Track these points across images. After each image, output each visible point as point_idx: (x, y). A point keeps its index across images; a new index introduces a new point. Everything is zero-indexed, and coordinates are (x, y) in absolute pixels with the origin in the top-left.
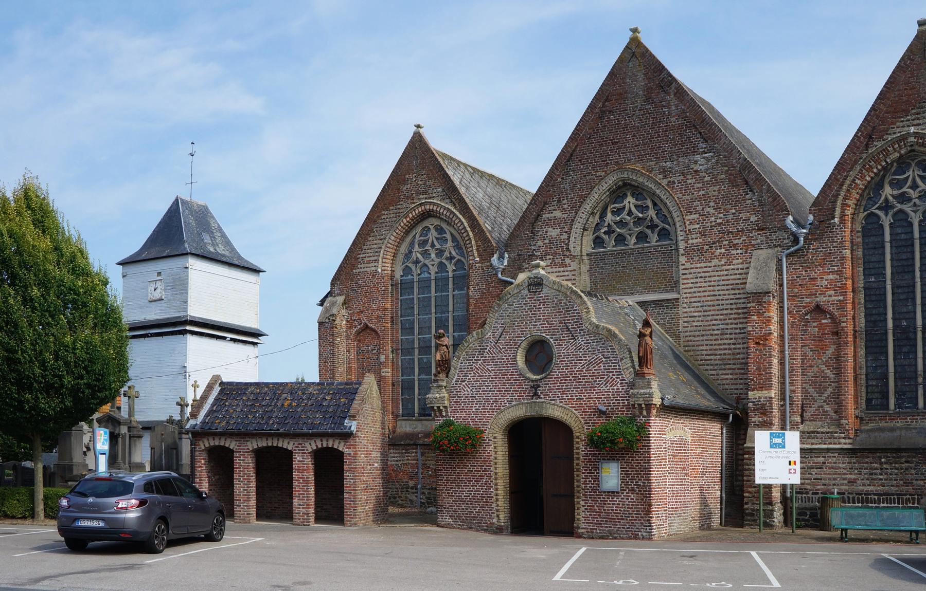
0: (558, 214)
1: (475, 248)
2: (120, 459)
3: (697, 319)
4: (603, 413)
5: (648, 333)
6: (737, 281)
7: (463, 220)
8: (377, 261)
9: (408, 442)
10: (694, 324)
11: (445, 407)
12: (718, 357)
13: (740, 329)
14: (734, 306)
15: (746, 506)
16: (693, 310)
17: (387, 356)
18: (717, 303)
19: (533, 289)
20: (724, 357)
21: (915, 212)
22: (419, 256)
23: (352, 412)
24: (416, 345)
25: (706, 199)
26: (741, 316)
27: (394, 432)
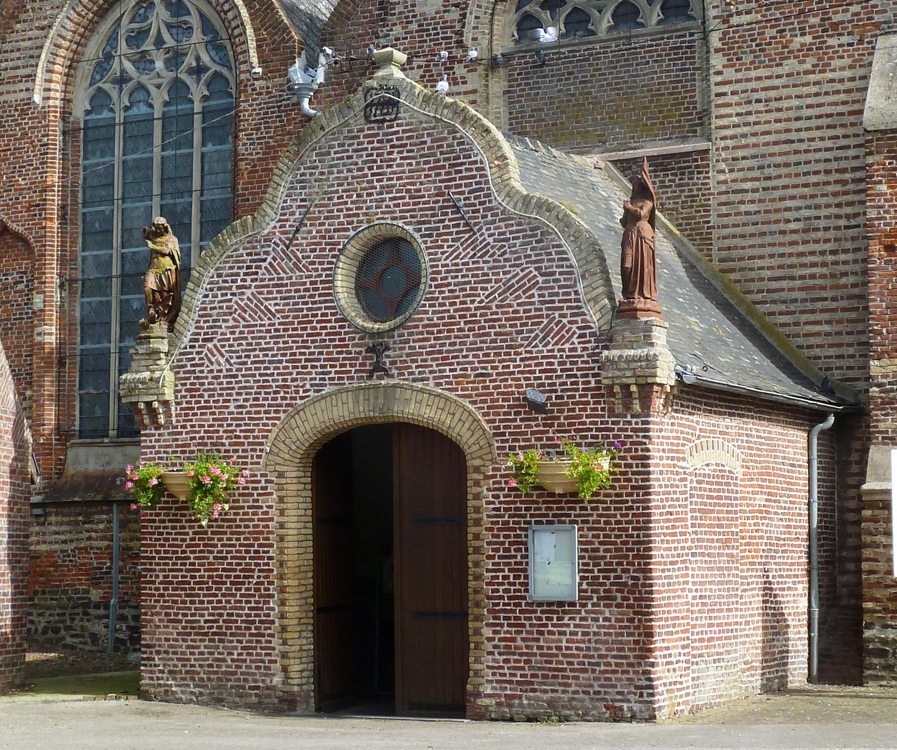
1: (252, 45)
3: (750, 196)
5: (645, 212)
6: (841, 109)
8: (31, 77)
9: (91, 496)
10: (743, 208)
11: (166, 403)
12: (798, 283)
13: (848, 217)
14: (834, 165)
15: (867, 634)
16: (740, 175)
18: (793, 158)
19: (377, 114)
20: (811, 282)
21: (158, 87)
22: (128, 65)
24: (115, 270)
26: (851, 187)
27: (60, 474)
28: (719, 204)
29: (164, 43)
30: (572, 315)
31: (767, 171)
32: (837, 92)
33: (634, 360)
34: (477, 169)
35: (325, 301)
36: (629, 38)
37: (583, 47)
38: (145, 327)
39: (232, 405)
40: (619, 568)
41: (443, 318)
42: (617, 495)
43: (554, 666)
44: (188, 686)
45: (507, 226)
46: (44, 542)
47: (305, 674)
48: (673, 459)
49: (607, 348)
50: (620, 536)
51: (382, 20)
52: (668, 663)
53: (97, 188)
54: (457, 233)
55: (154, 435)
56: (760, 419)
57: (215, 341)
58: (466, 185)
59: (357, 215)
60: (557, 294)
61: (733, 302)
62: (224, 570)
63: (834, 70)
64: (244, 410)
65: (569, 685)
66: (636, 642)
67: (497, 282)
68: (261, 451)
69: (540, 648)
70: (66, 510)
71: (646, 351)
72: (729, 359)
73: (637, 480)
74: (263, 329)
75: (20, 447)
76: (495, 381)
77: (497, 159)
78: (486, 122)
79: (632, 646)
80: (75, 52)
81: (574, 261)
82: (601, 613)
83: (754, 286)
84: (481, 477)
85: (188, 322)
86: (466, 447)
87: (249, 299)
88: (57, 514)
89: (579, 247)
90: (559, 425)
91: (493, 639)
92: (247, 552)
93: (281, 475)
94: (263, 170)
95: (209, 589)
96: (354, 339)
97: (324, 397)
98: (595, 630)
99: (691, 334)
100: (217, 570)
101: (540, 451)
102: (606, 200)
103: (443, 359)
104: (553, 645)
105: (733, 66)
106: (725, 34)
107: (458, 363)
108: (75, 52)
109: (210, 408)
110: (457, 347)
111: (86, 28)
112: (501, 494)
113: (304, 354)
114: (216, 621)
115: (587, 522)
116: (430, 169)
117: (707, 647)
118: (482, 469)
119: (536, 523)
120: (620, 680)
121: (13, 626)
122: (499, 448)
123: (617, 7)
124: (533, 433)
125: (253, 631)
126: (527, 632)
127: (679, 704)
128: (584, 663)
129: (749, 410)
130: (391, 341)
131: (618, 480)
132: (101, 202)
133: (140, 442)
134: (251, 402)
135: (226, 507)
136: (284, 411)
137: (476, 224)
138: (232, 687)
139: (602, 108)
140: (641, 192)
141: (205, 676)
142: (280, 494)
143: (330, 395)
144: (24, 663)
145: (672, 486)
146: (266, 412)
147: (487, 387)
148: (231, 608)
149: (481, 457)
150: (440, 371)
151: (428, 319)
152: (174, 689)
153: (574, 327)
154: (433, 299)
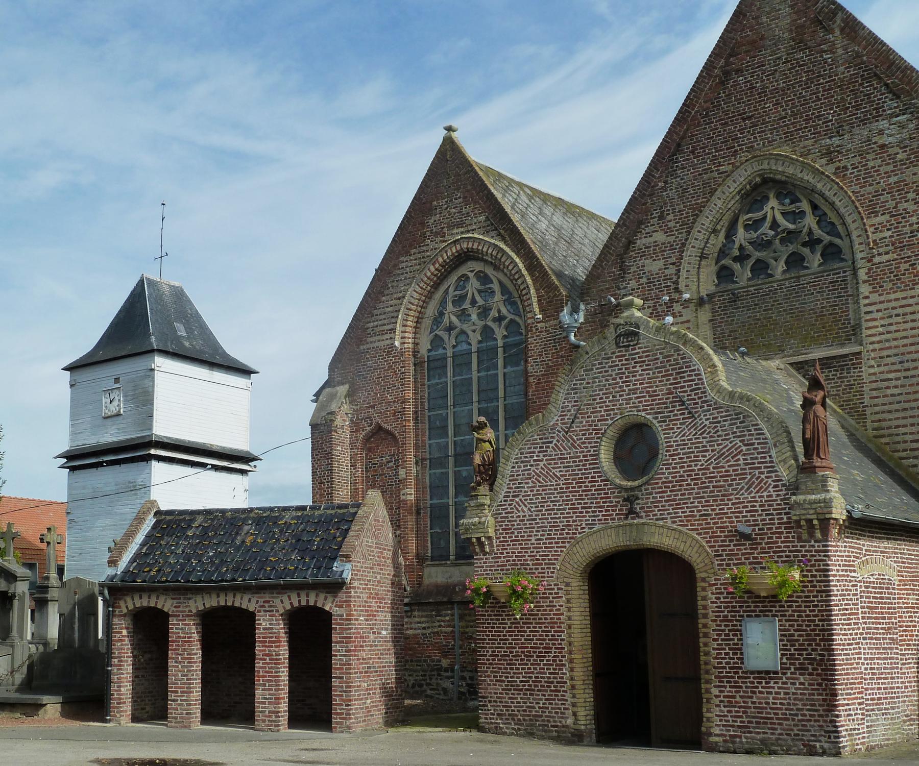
0: (660, 237)
1: (535, 300)
2: (14, 633)
3: (894, 383)
4: (747, 537)
5: (818, 399)
7: (517, 260)
8: (393, 330)
9: (440, 599)
10: (889, 392)
11: (489, 538)
16: (886, 368)
17: (410, 470)
19: (624, 341)
21: (474, 331)
22: (454, 319)
23: (344, 550)
24: (451, 452)
25: (901, 189)
27: (420, 584)
28: (871, 390)
29: (476, 302)
30: (768, 472)
31: (906, 365)
33: (811, 503)
34: (696, 375)
35: (594, 468)
36: (798, 277)
37: (764, 286)
38: (474, 489)
39: (533, 539)
40: (810, 648)
41: (676, 477)
42: (806, 597)
43: (764, 715)
44: (510, 724)
45: (718, 413)
46: (411, 629)
47: (588, 717)
48: (846, 571)
49: (794, 494)
50: (810, 626)
51: (622, 277)
52: (849, 715)
53: (438, 398)
54: (683, 419)
56: (910, 541)
57: (521, 497)
58: (689, 386)
59: (613, 410)
60: (757, 458)
61: (884, 459)
62: (531, 648)
65: (776, 729)
66: (824, 700)
67: (713, 451)
69: (753, 703)
70: (425, 608)
71: (823, 496)
72: (885, 499)
73: (820, 586)
75: (397, 568)
77: (709, 367)
78: (700, 342)
79: (821, 703)
80: (420, 312)
81: (768, 435)
82: (797, 679)
83: (900, 447)
84: (707, 584)
85: (503, 484)
86: (695, 564)
88: (418, 611)
89: (771, 425)
90: (762, 548)
91: (719, 696)
92: (547, 636)
93: (567, 585)
94: (545, 382)
95: (522, 660)
97: (595, 532)
98: (794, 691)
99: (854, 483)
100: (527, 647)
101: (749, 567)
102: (787, 390)
103: (677, 504)
105: (878, 291)
106: (870, 269)
108: (420, 312)
109: (519, 541)
111: (426, 297)
112: (721, 596)
113: (580, 504)
114: (528, 681)
115: (785, 615)
116: (662, 376)
117: (877, 704)
119: (748, 616)
120: (813, 726)
121: (396, 683)
122: (719, 565)
123: (789, 257)
124: (743, 554)
125: (553, 688)
126: (744, 692)
127: (857, 744)
129: (902, 536)
131: (807, 586)
132: (440, 407)
133: (474, 563)
135: (532, 606)
137: (696, 412)
138: (540, 725)
139: (781, 327)
140: (815, 384)
142: (568, 597)
143: (599, 530)
144: (404, 707)
145: (847, 590)
146: (556, 543)
147: (709, 524)
149: (706, 571)
150: (675, 513)
151: (666, 478)
153: (770, 480)
154: (668, 464)
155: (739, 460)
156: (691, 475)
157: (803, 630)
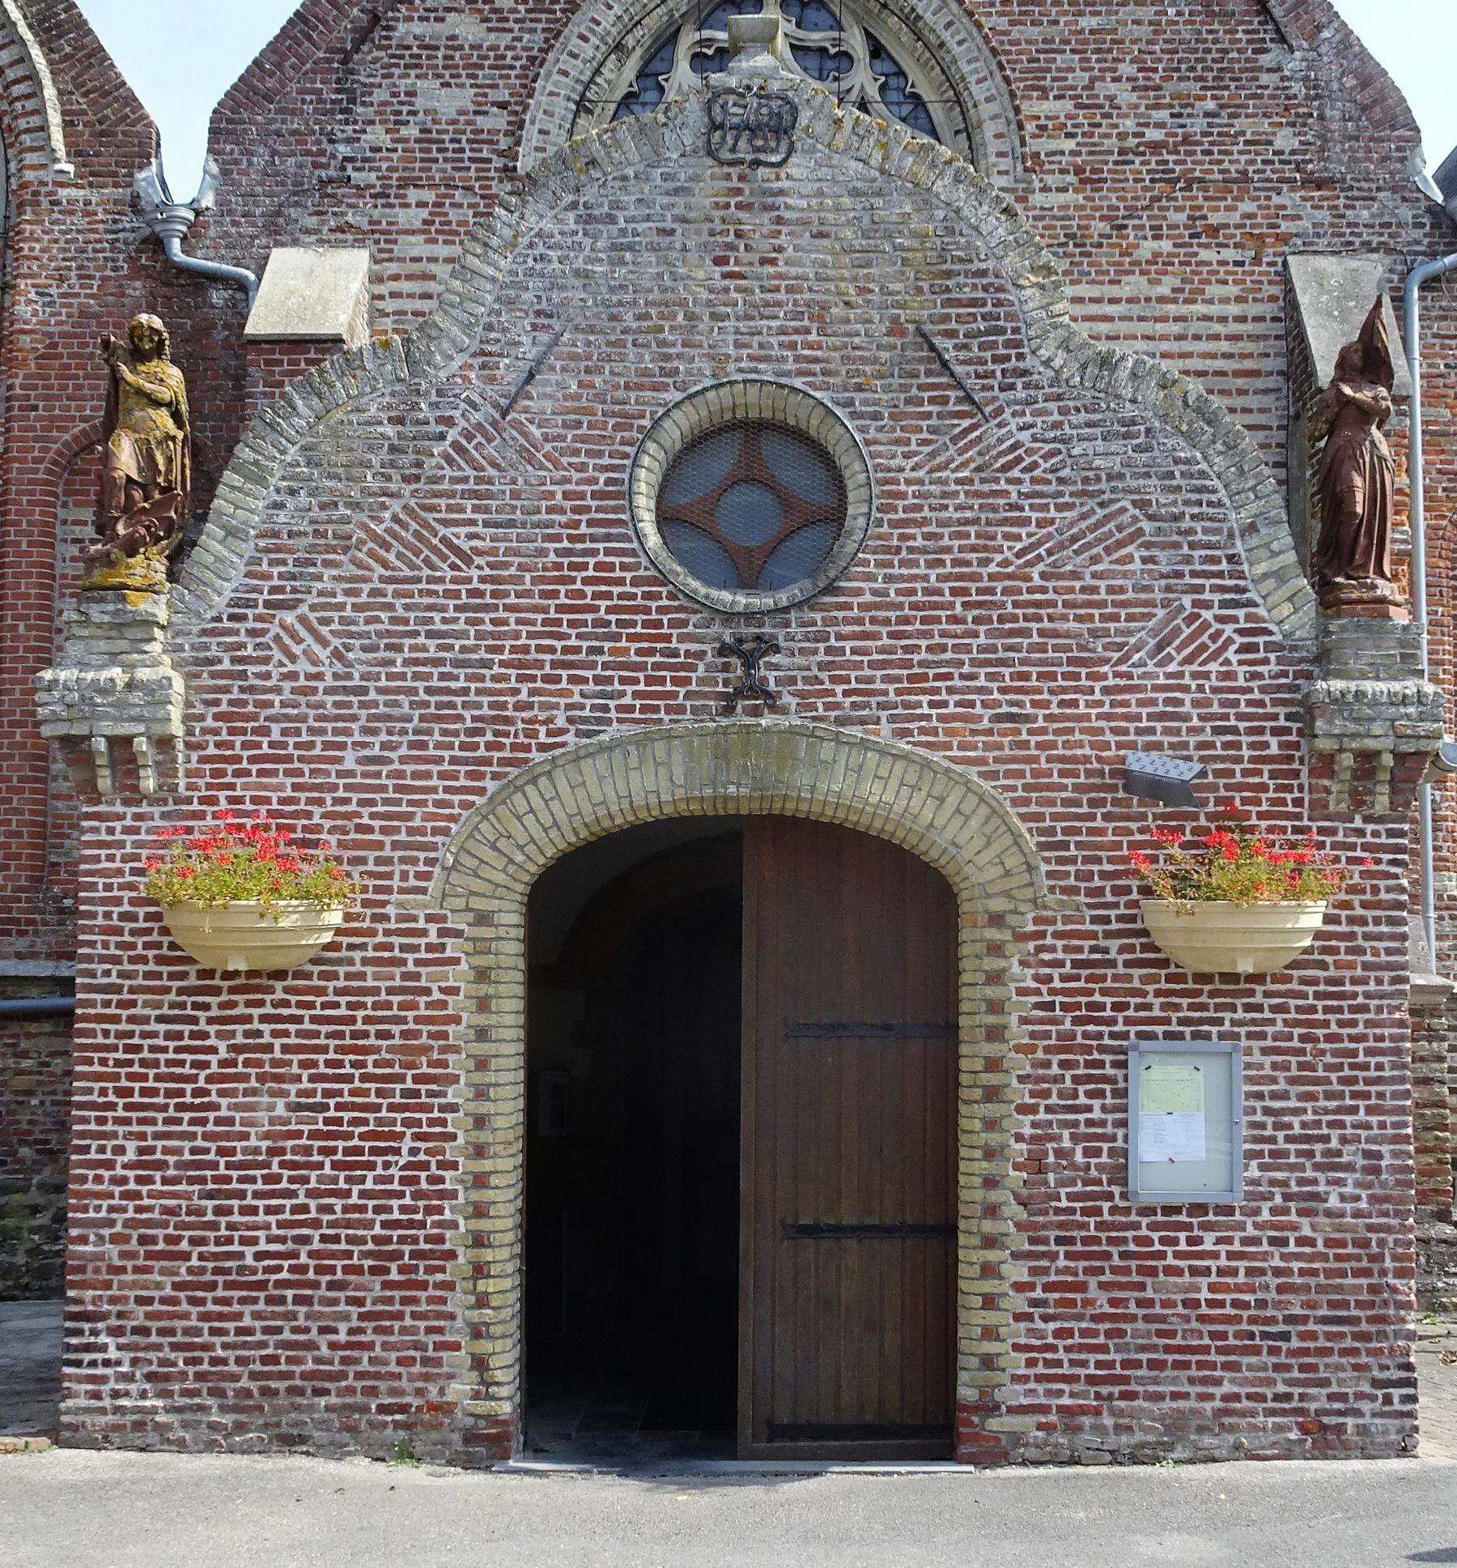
0: (468, 28)
1: (55, 118)
11: (164, 743)
30: (1224, 604)
32: (1216, 337)
41: (913, 592)
55: (120, 817)
57: (304, 609)
63: (1210, 302)
64: (385, 770)
67: (1040, 524)
68: (430, 862)
74: (439, 588)
76: (1043, 731)
79: (1365, 1297)
84: (1007, 935)
87: (396, 519)
91: (1031, 1287)
96: (684, 623)
97: (602, 748)
103: (912, 678)
104: (1179, 1297)
107: (951, 691)
110: (949, 655)
112: (1056, 973)
115: (1262, 1036)
118: (1011, 919)
119: (1141, 1035)
120: (1339, 1368)
122: (1050, 875)
128: (1252, 1336)
130: (781, 633)
134: (403, 751)
136: (496, 776)
141: (254, 1386)
142: (479, 961)
147: (1025, 745)
148: (332, 1224)
149: (1007, 894)
150: (907, 705)
151: (874, 592)
152: (161, 1418)
153: (1229, 629)
155: (1130, 559)
156: (965, 592)
157: (1317, 1081)
